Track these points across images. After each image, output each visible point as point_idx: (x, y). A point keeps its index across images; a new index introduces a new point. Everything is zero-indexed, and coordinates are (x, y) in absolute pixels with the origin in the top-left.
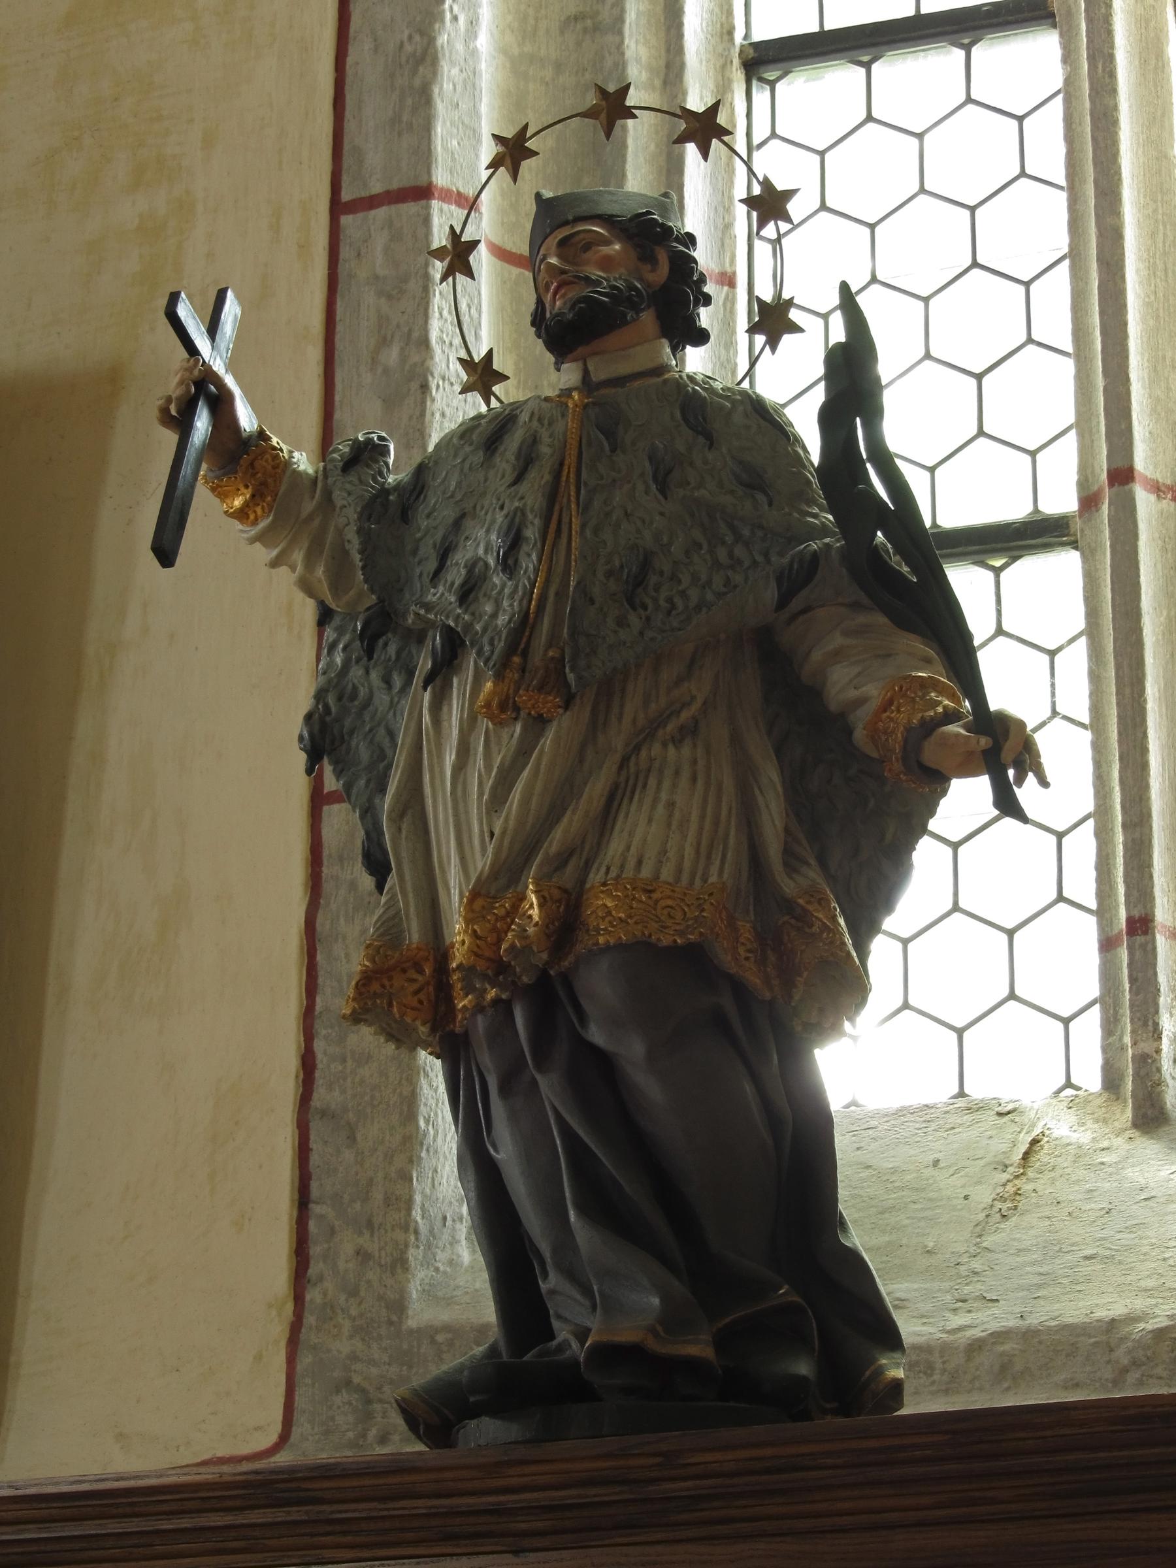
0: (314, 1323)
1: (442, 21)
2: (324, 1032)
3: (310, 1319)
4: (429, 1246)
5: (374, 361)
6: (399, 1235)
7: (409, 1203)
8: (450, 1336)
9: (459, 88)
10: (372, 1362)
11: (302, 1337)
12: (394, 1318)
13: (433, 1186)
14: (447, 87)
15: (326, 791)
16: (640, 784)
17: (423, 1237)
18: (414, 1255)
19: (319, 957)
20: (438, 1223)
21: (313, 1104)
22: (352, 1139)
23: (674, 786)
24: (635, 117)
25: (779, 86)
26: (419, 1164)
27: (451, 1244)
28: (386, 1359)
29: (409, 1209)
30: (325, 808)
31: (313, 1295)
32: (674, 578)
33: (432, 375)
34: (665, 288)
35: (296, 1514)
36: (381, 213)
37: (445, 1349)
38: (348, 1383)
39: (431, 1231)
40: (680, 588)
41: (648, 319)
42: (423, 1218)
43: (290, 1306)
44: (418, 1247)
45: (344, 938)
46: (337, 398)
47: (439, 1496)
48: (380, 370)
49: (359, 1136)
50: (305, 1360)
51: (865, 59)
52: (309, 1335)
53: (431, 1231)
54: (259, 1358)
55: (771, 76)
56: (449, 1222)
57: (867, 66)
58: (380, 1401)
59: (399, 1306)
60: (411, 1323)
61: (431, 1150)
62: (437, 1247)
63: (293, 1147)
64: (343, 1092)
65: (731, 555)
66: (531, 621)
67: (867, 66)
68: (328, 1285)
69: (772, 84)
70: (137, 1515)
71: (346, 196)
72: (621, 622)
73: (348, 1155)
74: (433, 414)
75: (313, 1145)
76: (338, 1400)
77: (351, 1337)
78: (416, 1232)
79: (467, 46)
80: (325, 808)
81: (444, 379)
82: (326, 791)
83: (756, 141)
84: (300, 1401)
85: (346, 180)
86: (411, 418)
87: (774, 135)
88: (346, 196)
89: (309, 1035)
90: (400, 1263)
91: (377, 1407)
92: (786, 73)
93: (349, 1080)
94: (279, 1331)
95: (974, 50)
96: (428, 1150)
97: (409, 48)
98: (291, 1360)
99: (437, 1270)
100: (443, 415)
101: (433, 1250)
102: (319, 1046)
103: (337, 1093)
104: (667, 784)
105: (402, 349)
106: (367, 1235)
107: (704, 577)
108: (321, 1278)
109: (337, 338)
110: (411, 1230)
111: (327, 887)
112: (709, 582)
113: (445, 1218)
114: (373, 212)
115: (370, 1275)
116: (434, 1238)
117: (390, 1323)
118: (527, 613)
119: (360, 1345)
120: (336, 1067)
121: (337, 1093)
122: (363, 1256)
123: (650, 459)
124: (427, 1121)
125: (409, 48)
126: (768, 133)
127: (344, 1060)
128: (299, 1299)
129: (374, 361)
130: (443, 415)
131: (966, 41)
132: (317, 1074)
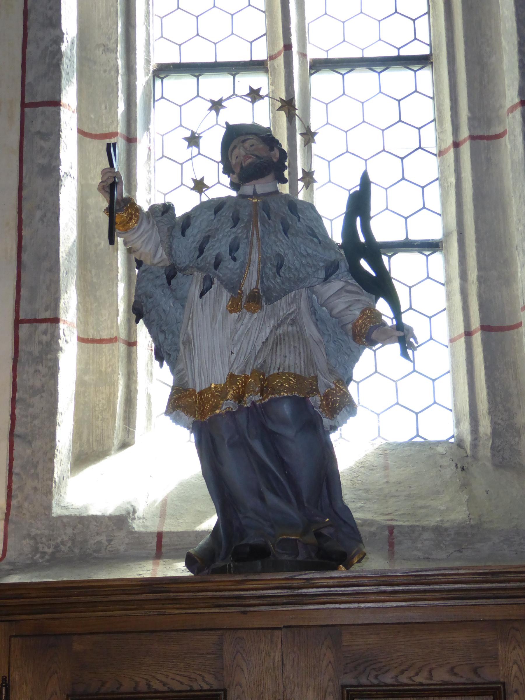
0: (15, 514)
1: (63, 42)
2: (19, 407)
3: (13, 512)
4: (59, 487)
9: (69, 66)
12: (47, 513)
14: (65, 66)
15: (20, 319)
16: (282, 339)
17: (57, 484)
19: (17, 379)
21: (14, 433)
23: (294, 341)
24: (280, 98)
25: (164, 80)
30: (20, 325)
31: (14, 502)
35: (158, 596)
36: (40, 109)
38: (29, 535)
45: (28, 373)
46: (24, 175)
47: (216, 591)
50: (11, 527)
51: (197, 74)
53: (60, 481)
55: (162, 76)
56: (65, 478)
57: (198, 77)
58: (42, 543)
60: (54, 515)
67: (198, 77)
68: (19, 498)
69: (162, 79)
70: (126, 594)
71: (27, 101)
76: (24, 542)
79: (71, 52)
80: (20, 325)
82: (20, 319)
83: (156, 99)
84: (10, 541)
85: (26, 94)
87: (162, 97)
88: (27, 101)
89: (13, 408)
92: (167, 76)
93: (29, 425)
95: (236, 76)
97: (51, 49)
102: (17, 411)
104: (292, 340)
106: (36, 481)
109: (24, 153)
111: (21, 354)
113: (64, 477)
114: (37, 108)
117: (46, 514)
123: (282, 223)
125: (51, 49)
126: (161, 96)
131: (234, 73)
132: (16, 422)
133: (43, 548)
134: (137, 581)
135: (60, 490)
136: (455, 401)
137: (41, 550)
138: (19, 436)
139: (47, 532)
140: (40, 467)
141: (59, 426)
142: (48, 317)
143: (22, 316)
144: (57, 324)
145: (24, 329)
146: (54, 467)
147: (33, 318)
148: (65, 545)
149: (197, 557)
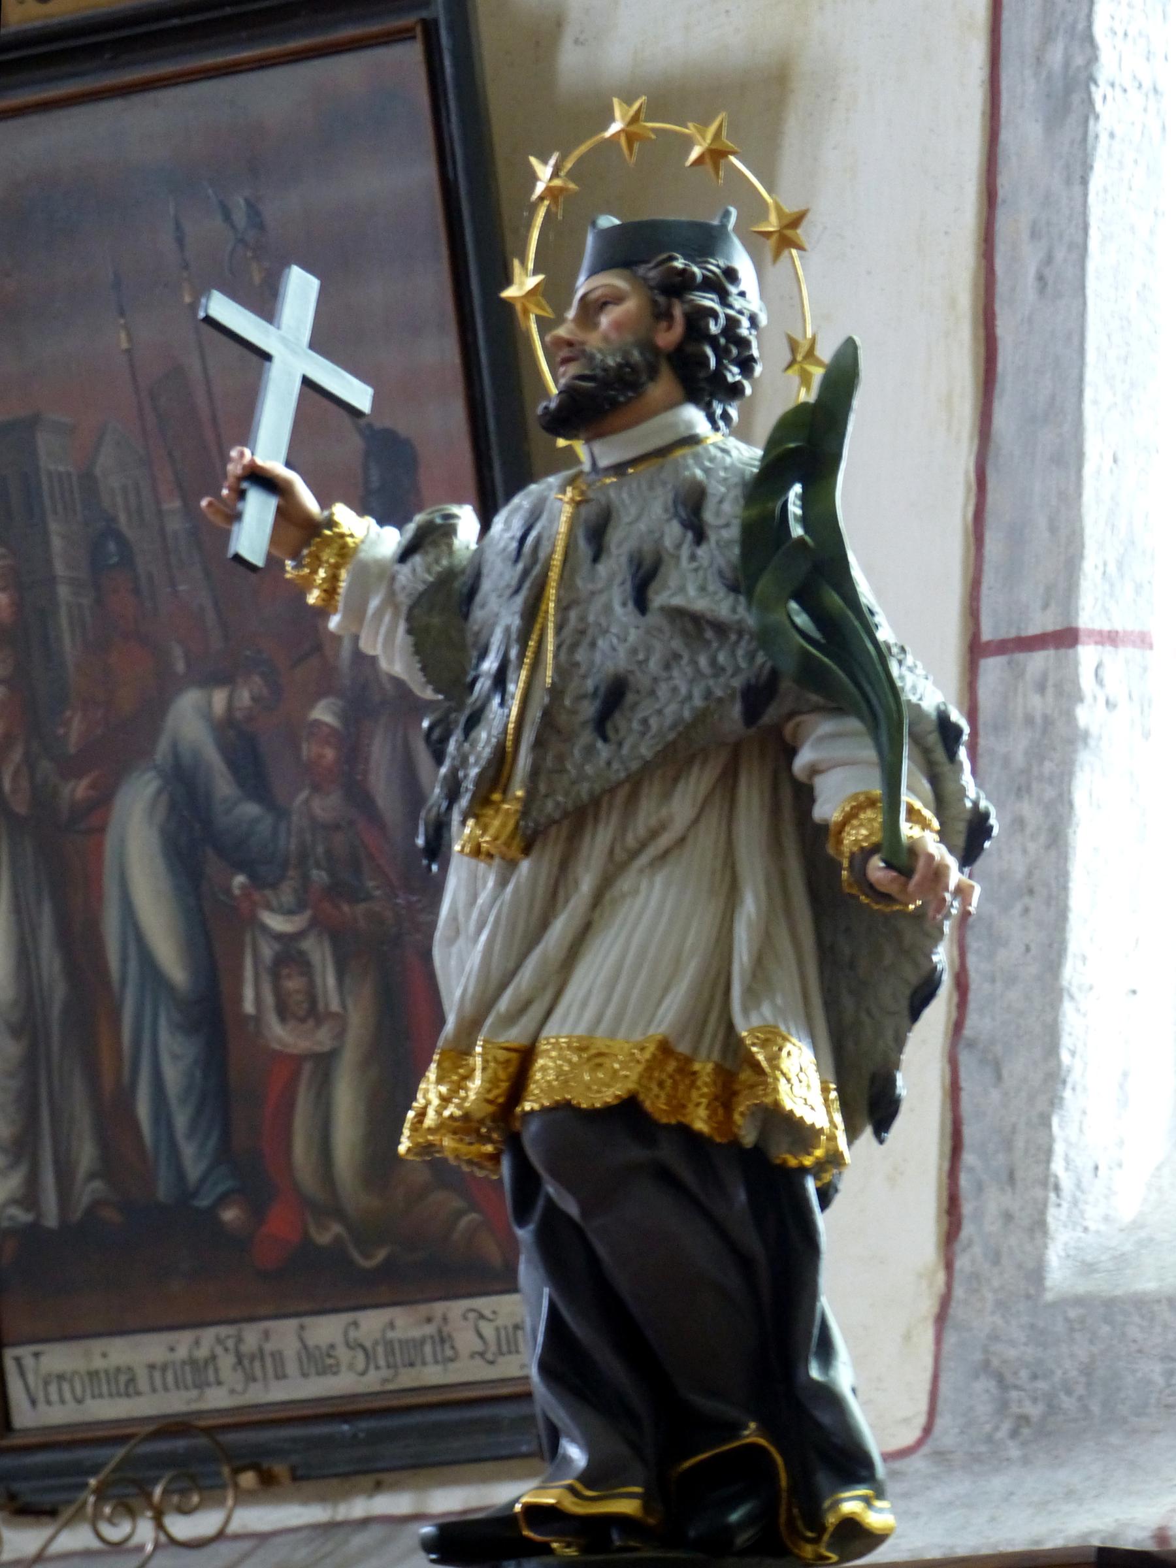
4: (1075, 1203)
5: (1039, 61)
6: (1038, 1192)
7: (1049, 1153)
8: (1081, 1311)
10: (1012, 1343)
11: (951, 1311)
12: (1032, 1291)
13: (1081, 1130)
18: (1055, 1217)
20: (1088, 1175)
22: (999, 1078)
26: (1061, 1106)
27: (1107, 1197)
28: (1023, 1339)
29: (1048, 1161)
31: (962, 1263)
32: (652, 693)
33: (1096, 83)
34: (679, 349)
37: (1077, 1326)
39: (1078, 1185)
40: (657, 706)
41: (663, 386)
42: (1067, 1169)
43: (941, 1277)
44: (1059, 1205)
48: (1044, 75)
49: (1005, 1073)
50: (951, 1339)
52: (957, 1311)
53: (1078, 1185)
54: (907, 1337)
59: (1037, 1274)
61: (1079, 1088)
62: (1086, 1203)
63: (943, 1087)
64: (993, 1019)
65: (713, 662)
66: (509, 750)
68: (977, 1250)
72: (590, 751)
73: (995, 1095)
74: (1097, 137)
75: (964, 1083)
77: (993, 1313)
78: (1057, 1188)
81: (1113, 85)
82: (1049, 1297)
84: (944, 1388)
86: (1072, 142)
90: (1039, 1227)
91: (1014, 1394)
94: (928, 1306)
96: (1074, 1089)
98: (939, 1340)
99: (1086, 1229)
100: (1112, 135)
101: (1081, 1206)
102: (972, 960)
103: (987, 1020)
105: (1066, 49)
107: (683, 690)
108: (970, 1244)
110: (1051, 1186)
112: (690, 697)
115: (1013, 1241)
116: (1083, 1192)
117: (1028, 1297)
118: (504, 747)
119: (999, 1322)
120: (987, 986)
121: (987, 1020)
122: (1008, 1217)
124: (1073, 1053)
127: (993, 980)
128: (949, 1266)
129: (1039, 61)
130: (1112, 135)
133: (1020, 1401)
134: (783, 876)
135: (1082, 1213)
136: (403, 1468)
137: (1015, 1409)
138: (971, 1045)
139: (1030, 1352)
140: (1020, 1143)
141: (1072, 997)
142: (1050, 628)
143: (986, 635)
144: (1071, 651)
145: (992, 668)
146: (1051, 1139)
147: (1013, 634)
148: (1069, 1392)
149: (174, 745)
